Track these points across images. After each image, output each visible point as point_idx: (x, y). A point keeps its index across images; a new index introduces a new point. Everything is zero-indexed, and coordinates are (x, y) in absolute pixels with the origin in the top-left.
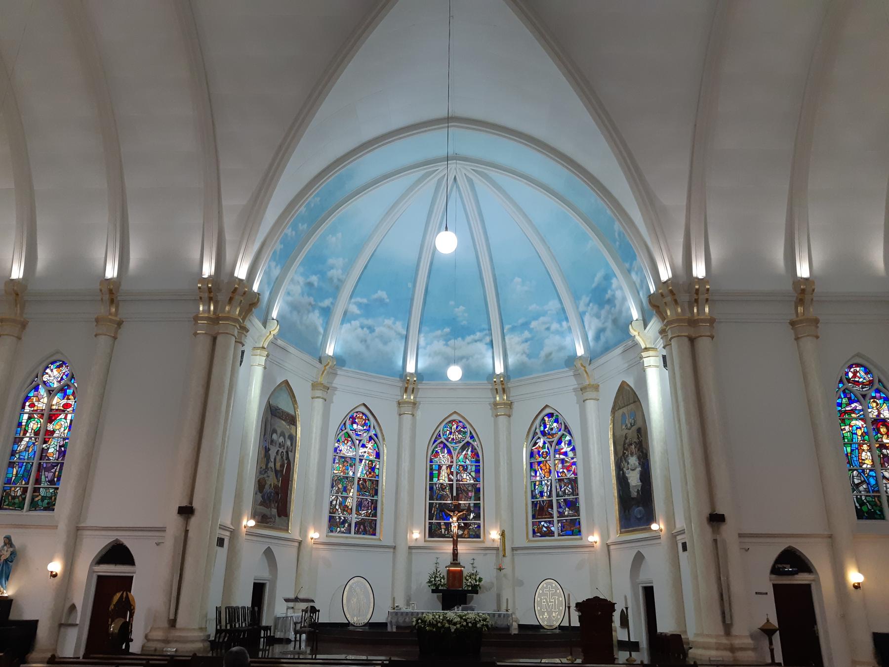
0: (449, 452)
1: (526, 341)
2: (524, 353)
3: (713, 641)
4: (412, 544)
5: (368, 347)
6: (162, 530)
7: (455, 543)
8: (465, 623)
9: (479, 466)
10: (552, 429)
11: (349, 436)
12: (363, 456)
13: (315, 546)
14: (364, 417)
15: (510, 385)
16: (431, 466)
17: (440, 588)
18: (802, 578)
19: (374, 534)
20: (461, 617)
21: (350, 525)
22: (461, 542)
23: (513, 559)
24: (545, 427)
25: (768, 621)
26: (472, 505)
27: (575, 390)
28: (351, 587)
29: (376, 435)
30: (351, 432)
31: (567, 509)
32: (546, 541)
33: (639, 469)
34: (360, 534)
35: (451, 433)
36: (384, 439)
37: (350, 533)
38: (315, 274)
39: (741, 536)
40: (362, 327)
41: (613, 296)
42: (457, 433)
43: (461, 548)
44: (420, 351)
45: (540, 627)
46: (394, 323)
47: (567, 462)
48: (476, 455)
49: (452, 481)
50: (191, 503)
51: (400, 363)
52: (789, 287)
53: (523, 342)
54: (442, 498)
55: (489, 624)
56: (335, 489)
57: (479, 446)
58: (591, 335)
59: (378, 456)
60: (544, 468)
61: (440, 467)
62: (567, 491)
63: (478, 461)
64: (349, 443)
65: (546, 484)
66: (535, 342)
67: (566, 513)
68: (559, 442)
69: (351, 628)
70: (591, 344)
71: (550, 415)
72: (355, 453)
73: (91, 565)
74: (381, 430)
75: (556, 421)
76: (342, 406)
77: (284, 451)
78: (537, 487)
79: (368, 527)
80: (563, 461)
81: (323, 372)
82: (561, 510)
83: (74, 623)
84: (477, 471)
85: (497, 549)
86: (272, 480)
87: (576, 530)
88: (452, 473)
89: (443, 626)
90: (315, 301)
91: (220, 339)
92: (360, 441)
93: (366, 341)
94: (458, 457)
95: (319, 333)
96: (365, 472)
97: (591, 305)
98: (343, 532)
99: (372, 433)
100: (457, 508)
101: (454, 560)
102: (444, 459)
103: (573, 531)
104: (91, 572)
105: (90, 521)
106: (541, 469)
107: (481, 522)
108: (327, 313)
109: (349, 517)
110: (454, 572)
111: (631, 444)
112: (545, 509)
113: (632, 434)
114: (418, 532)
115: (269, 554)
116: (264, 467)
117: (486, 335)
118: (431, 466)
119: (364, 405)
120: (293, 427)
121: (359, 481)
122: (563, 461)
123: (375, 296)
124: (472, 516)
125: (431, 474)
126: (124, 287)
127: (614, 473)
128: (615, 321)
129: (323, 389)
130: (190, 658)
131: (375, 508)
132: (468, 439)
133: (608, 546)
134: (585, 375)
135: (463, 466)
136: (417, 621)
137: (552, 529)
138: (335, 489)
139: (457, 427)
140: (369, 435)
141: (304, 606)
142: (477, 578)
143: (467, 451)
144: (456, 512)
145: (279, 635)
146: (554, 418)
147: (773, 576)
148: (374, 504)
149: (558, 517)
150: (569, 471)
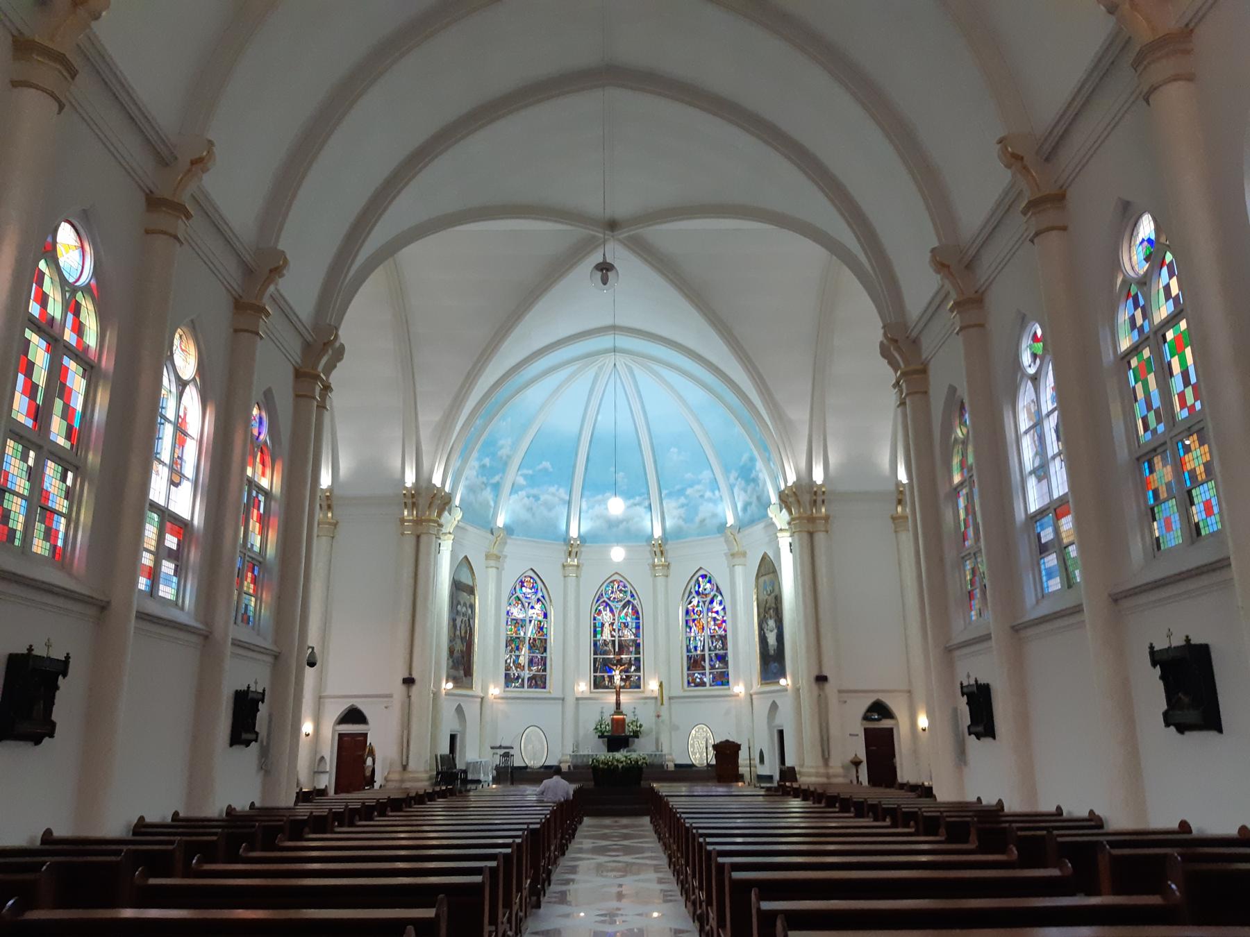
0: (612, 611)
1: (682, 506)
2: (680, 517)
3: (813, 770)
4: (579, 696)
5: (533, 515)
6: (390, 696)
7: (618, 694)
8: (629, 762)
9: (639, 623)
10: (705, 589)
11: (519, 600)
12: (532, 617)
13: (495, 700)
14: (532, 581)
15: (667, 547)
16: (595, 624)
17: (606, 734)
18: (886, 723)
19: (544, 688)
20: (626, 757)
21: (523, 680)
22: (623, 692)
23: (670, 709)
24: (699, 587)
25: (856, 755)
26: (633, 659)
27: (725, 554)
28: (527, 736)
29: (543, 597)
30: (521, 596)
31: (718, 662)
32: (700, 691)
33: (776, 631)
34: (532, 688)
35: (612, 592)
36: (551, 601)
37: (523, 687)
38: (488, 456)
39: (840, 692)
40: (528, 497)
41: (757, 476)
42: (618, 592)
43: (623, 698)
44: (582, 514)
45: (693, 765)
46: (558, 490)
47: (718, 620)
48: (636, 612)
49: (614, 637)
50: (410, 674)
51: (564, 527)
52: (892, 487)
53: (679, 507)
54: (605, 653)
55: (648, 762)
56: (509, 648)
57: (639, 603)
58: (740, 506)
59: (545, 616)
60: (698, 625)
61: (603, 625)
62: (718, 646)
63: (638, 618)
64: (520, 606)
65: (700, 640)
66: (690, 509)
67: (717, 666)
68: (712, 602)
69: (528, 770)
70: (740, 514)
71: (704, 576)
72: (524, 615)
73: (334, 725)
74: (548, 593)
75: (710, 582)
76: (513, 570)
77: (467, 619)
78: (691, 642)
79: (538, 681)
80: (715, 619)
81: (496, 543)
82: (712, 663)
83: (323, 770)
84: (638, 628)
85: (656, 698)
86: (459, 646)
87: (725, 681)
88: (614, 630)
89: (612, 764)
90: (487, 479)
91: (424, 539)
92: (529, 603)
93: (531, 509)
94: (619, 615)
95: (490, 506)
96: (534, 632)
97: (739, 479)
98: (517, 687)
99: (540, 595)
100: (620, 662)
101: (617, 709)
102: (606, 616)
103: (722, 682)
104: (334, 731)
105: (328, 692)
106: (696, 626)
107: (641, 674)
108: (497, 487)
109: (522, 674)
110: (617, 720)
111: (770, 609)
112: (699, 662)
113: (771, 599)
114: (584, 684)
115: (459, 710)
116: (453, 636)
117: (644, 499)
118: (595, 624)
119: (532, 569)
120: (472, 596)
121: (529, 641)
122: (715, 619)
123: (541, 467)
124: (633, 668)
125: (595, 631)
126: (336, 492)
127: (757, 632)
128: (759, 498)
129: (495, 558)
130: (385, 801)
131: (545, 664)
132: (629, 598)
133: (751, 695)
134: (735, 543)
135: (624, 623)
136: (593, 761)
137: (705, 680)
138: (509, 648)
139: (618, 587)
140: (537, 597)
141: (502, 751)
142: (638, 725)
143: (628, 609)
144: (619, 666)
145: (470, 777)
146: (708, 579)
147: (865, 722)
148: (544, 660)
149: (710, 669)
150: (720, 628)
